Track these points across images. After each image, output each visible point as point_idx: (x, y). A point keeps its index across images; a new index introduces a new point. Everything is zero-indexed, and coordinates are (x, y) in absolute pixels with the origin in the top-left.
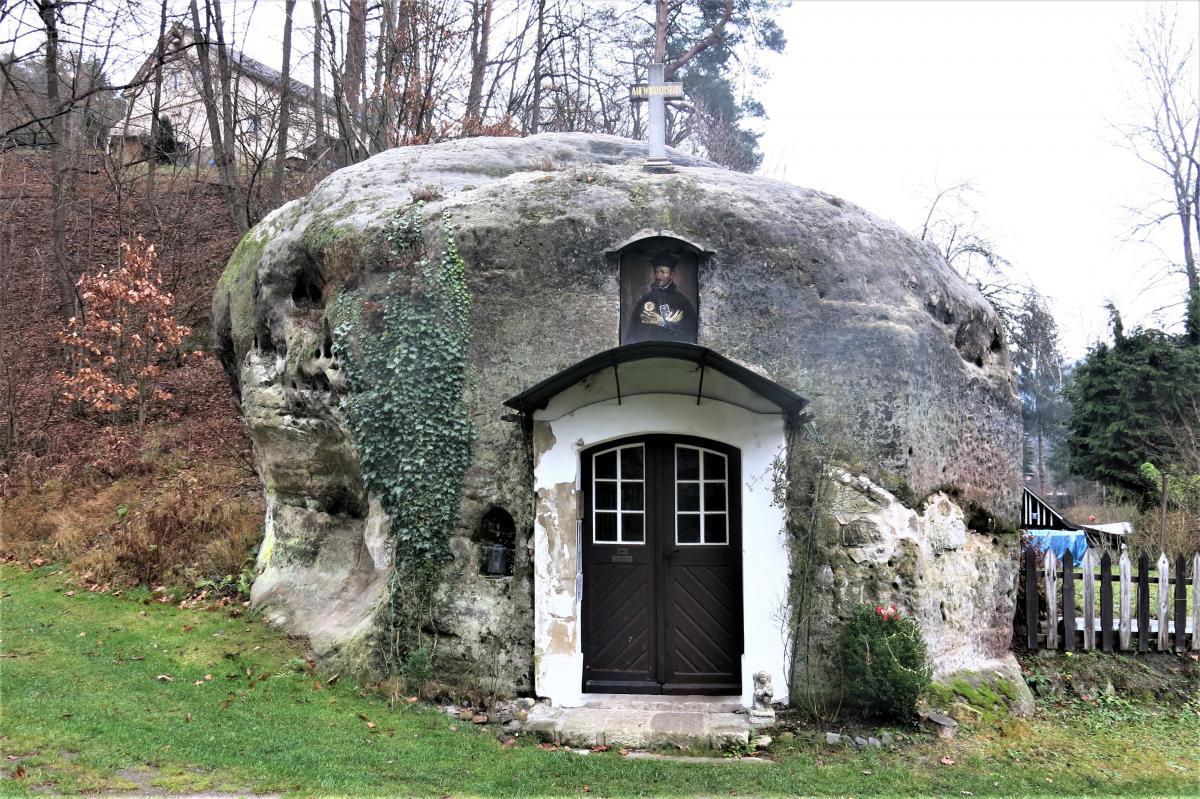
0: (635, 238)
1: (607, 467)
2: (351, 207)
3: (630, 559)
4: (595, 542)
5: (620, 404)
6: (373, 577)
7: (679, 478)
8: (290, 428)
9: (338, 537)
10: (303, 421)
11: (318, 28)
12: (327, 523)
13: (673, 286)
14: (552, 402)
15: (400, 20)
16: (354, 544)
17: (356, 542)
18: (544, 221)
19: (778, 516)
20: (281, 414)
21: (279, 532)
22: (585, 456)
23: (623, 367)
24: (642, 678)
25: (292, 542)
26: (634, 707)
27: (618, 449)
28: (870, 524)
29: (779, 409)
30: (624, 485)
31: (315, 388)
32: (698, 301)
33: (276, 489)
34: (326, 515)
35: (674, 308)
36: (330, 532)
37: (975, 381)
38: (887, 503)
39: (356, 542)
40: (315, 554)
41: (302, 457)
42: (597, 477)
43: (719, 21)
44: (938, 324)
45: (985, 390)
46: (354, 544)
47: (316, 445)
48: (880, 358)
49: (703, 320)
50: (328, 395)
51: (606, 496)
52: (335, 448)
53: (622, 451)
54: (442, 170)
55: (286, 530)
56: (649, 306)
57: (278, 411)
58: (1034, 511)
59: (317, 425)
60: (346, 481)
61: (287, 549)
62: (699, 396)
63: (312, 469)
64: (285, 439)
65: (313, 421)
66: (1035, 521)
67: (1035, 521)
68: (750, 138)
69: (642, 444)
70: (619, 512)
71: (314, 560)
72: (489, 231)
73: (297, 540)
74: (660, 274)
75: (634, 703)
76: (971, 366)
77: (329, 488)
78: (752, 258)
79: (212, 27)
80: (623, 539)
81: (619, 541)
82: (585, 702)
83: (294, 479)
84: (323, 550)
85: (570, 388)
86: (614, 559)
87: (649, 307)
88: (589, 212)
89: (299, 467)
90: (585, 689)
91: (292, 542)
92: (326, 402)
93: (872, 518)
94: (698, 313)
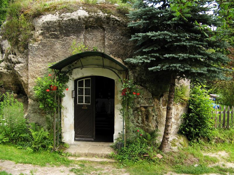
1: (81, 84)
7: (79, 95)
8: (6, 72)
10: (9, 71)
18: (65, 19)
20: (4, 69)
24: (89, 138)
27: (84, 80)
34: (16, 94)
35: (181, 60)
41: (10, 80)
42: (78, 87)
43: (159, 22)
51: (81, 91)
57: (3, 68)
65: (11, 71)
69: (90, 78)
72: (51, 22)
75: (86, 144)
78: (119, 30)
83: (8, 85)
86: (83, 108)
89: (9, 82)
90: (75, 140)
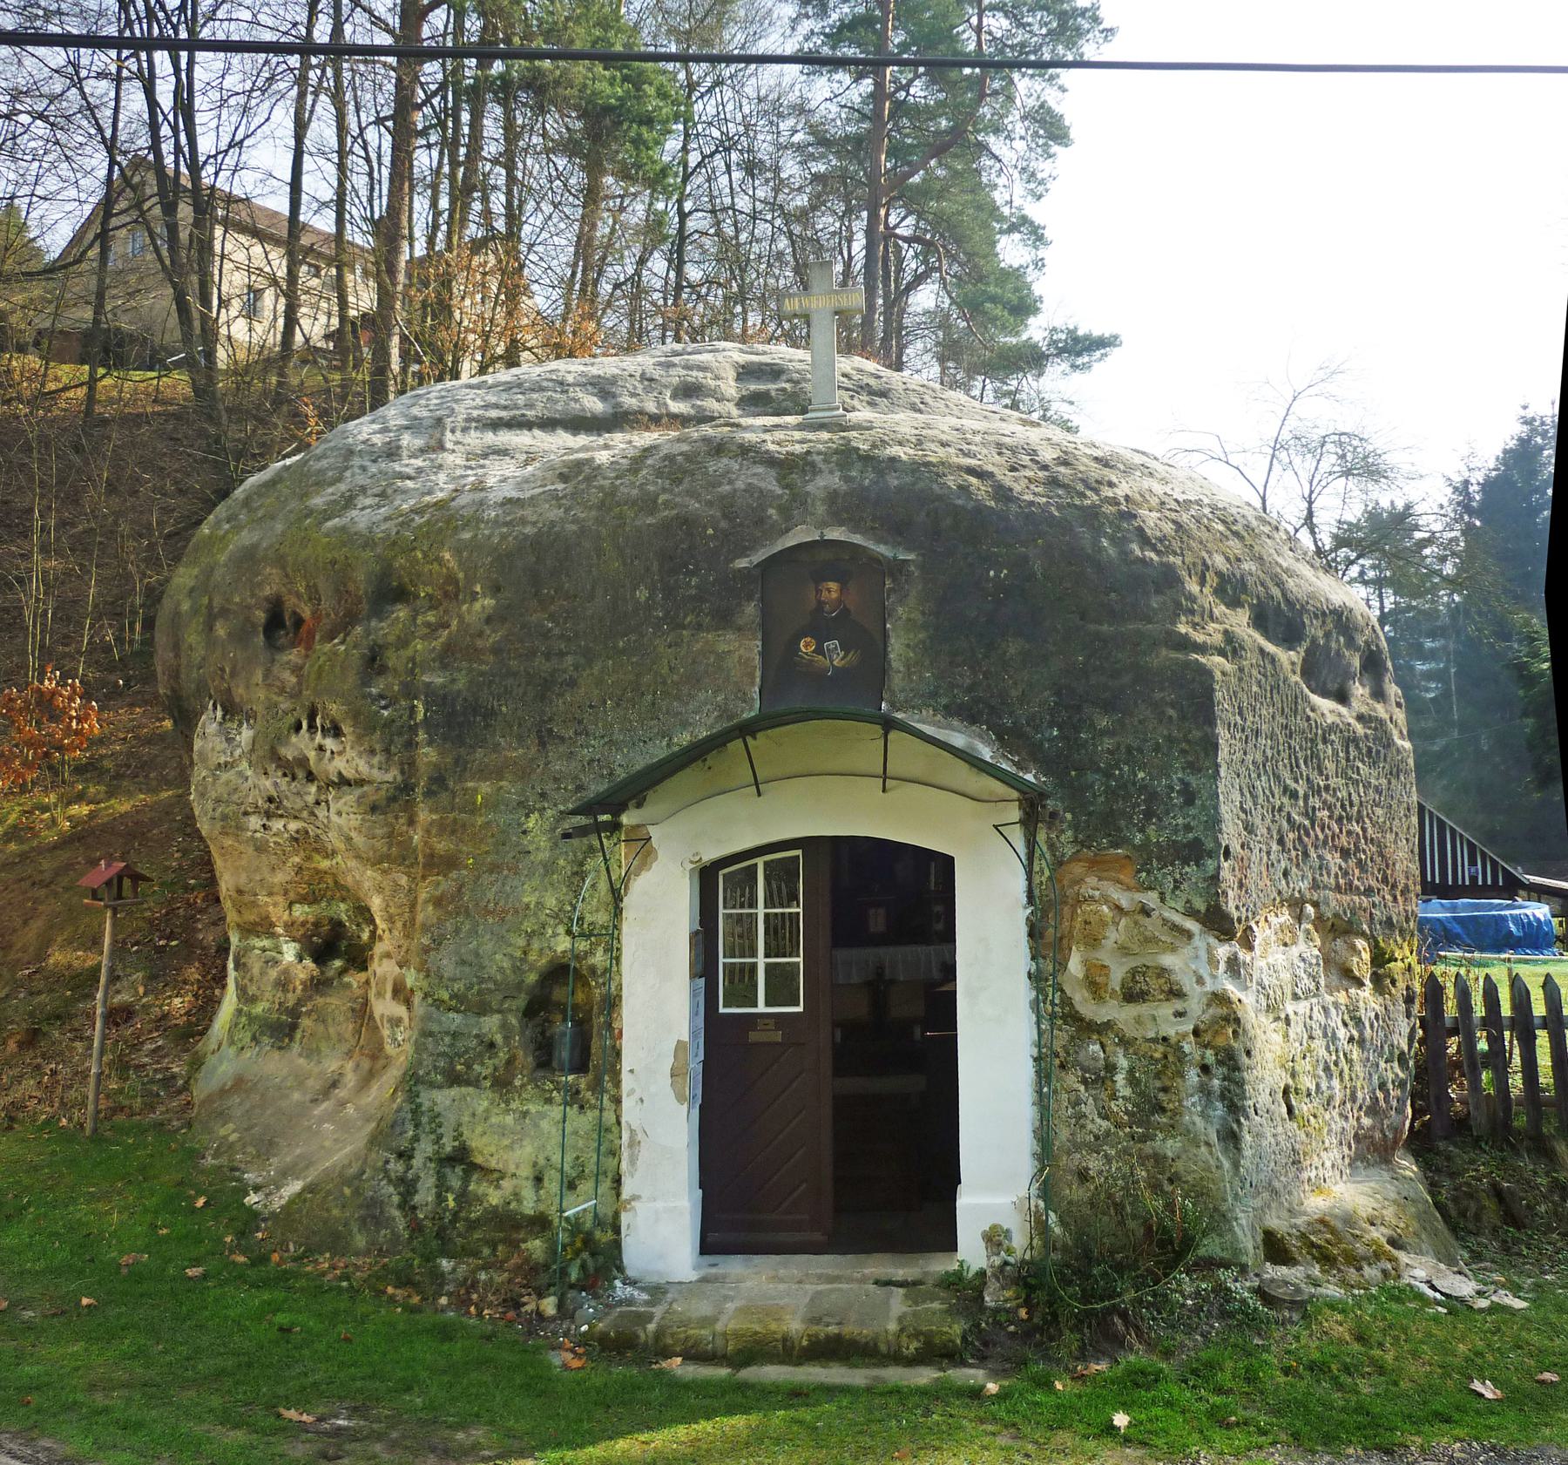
0: (790, 541)
2: (349, 501)
3: (778, 1037)
4: (722, 1010)
5: (759, 794)
6: (381, 1062)
8: (258, 835)
9: (328, 1000)
10: (277, 825)
11: (342, 153)
12: (312, 978)
13: (845, 612)
14: (650, 795)
15: (114, 935)
16: (353, 1010)
17: (358, 1007)
19: (1016, 955)
21: (242, 991)
22: (707, 876)
23: (758, 743)
25: (259, 1009)
26: (781, 1280)
27: (760, 862)
28: (1162, 972)
29: (1015, 794)
30: (754, 954)
31: (294, 778)
32: (885, 635)
33: (238, 925)
36: (317, 991)
37: (1333, 728)
38: (1189, 935)
39: (358, 1007)
40: (293, 1027)
44: (1270, 648)
45: (1351, 740)
46: (353, 1010)
47: (297, 859)
48: (1173, 707)
49: (894, 664)
50: (313, 789)
52: (325, 864)
53: (766, 864)
54: (496, 425)
55: (252, 990)
56: (806, 646)
58: (1473, 862)
59: (297, 832)
60: (342, 910)
61: (252, 1019)
62: (885, 777)
63: (292, 895)
64: (251, 850)
66: (1474, 879)
67: (1474, 879)
68: (1014, 276)
69: (799, 852)
70: (761, 961)
71: (291, 1039)
73: (267, 1005)
74: (825, 593)
75: (782, 1272)
76: (1325, 705)
77: (317, 924)
79: (184, 170)
80: (768, 1004)
81: (761, 1008)
82: (702, 1273)
84: (305, 1022)
85: (688, 770)
86: (754, 1036)
87: (806, 646)
88: (710, 504)
91: (259, 1009)
92: (310, 799)
93: (1168, 960)
94: (885, 653)
